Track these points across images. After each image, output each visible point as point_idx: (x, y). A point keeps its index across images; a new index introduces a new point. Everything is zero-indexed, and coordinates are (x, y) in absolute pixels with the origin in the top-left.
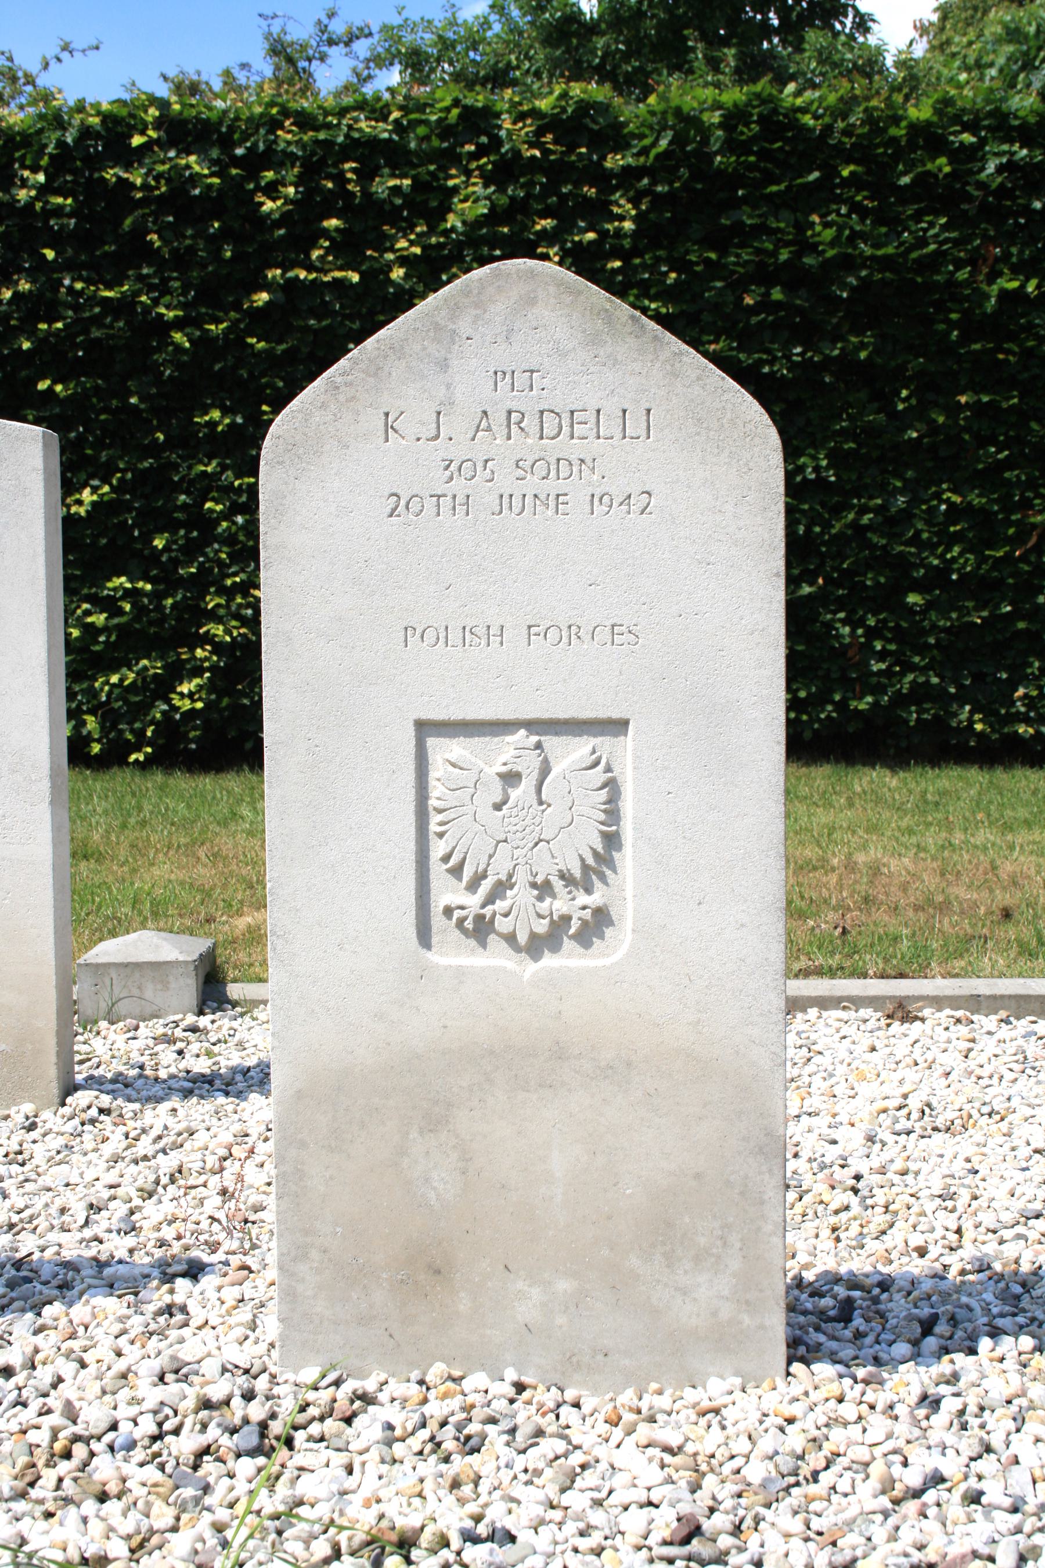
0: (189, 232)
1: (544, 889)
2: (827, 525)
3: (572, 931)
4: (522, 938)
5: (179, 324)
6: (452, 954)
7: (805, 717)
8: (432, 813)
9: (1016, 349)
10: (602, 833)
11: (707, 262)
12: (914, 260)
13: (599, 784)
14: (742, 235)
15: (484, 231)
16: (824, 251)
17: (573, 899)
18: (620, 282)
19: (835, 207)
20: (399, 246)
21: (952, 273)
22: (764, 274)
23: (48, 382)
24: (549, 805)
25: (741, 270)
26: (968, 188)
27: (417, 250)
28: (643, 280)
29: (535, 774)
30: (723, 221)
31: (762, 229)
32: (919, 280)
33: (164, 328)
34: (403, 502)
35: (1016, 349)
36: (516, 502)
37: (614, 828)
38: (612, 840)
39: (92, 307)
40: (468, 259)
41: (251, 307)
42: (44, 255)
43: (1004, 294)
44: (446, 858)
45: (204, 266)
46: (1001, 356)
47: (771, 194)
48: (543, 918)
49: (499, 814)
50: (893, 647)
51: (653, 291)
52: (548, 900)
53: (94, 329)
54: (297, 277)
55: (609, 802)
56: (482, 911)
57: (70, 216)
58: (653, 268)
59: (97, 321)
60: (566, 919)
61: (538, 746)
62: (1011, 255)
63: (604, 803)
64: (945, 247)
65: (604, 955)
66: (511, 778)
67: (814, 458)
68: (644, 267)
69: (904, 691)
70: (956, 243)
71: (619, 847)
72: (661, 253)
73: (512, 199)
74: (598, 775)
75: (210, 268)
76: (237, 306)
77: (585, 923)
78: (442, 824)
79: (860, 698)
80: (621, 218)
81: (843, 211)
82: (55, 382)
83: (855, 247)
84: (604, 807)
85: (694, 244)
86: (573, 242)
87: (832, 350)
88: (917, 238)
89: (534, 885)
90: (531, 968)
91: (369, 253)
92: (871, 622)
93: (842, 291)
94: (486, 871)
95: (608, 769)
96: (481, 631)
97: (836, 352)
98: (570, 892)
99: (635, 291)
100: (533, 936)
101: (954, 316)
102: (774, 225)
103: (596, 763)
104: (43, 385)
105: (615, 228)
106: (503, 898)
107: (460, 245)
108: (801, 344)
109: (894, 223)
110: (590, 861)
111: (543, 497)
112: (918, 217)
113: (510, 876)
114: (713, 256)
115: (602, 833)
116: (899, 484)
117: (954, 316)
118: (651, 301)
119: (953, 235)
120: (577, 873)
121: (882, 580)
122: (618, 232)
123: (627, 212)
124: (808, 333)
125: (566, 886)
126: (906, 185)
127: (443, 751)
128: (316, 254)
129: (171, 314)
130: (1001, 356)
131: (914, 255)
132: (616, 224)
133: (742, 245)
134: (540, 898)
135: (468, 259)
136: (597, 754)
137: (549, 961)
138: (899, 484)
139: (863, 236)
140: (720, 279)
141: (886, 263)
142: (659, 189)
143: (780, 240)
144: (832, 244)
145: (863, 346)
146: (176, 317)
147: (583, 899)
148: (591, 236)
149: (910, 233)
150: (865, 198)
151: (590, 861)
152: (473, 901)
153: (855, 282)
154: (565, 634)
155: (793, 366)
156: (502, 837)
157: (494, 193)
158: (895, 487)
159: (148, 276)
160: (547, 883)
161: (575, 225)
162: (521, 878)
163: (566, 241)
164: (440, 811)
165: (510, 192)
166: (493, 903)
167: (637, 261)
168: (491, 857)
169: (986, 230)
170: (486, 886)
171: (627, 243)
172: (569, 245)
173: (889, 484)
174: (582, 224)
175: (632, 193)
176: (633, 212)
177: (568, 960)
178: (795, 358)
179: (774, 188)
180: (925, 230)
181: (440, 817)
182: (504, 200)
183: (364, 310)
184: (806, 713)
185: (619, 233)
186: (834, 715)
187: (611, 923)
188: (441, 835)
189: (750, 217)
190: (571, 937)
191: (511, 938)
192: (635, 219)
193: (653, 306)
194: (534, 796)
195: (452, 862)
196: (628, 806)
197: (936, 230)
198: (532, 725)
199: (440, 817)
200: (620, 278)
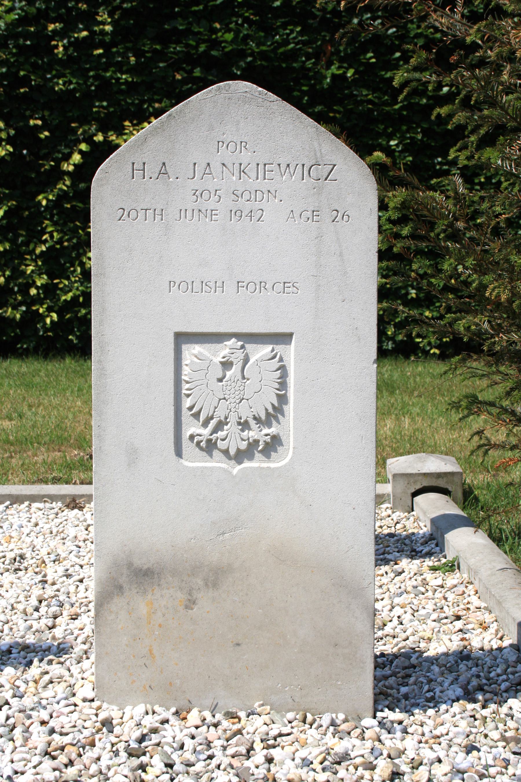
3: (260, 448)
4: (232, 452)
6: (194, 461)
9: (342, 109)
10: (277, 395)
11: (155, 51)
12: (282, 53)
13: (275, 369)
14: (178, 36)
15: (20, 29)
16: (225, 47)
17: (261, 431)
21: (304, 62)
24: (248, 379)
25: (176, 57)
26: (313, 10)
28: (118, 62)
29: (240, 364)
31: (188, 32)
32: (284, 65)
34: (126, 213)
35: (342, 109)
36: (189, 213)
37: (283, 392)
38: (283, 399)
43: (334, 76)
44: (191, 408)
46: (331, 115)
47: (195, 11)
48: (245, 440)
51: (124, 68)
52: (246, 432)
56: (211, 437)
60: (257, 442)
61: (243, 347)
62: (340, 51)
63: (278, 379)
64: (298, 47)
66: (227, 365)
70: (304, 43)
72: (129, 45)
73: (39, 10)
74: (275, 364)
77: (266, 443)
80: (104, 23)
81: (240, 22)
83: (248, 44)
84: (279, 380)
86: (74, 37)
88: (283, 40)
89: (239, 424)
94: (213, 415)
96: (212, 284)
98: (259, 427)
99: (113, 69)
100: (239, 451)
101: (305, 88)
102: (196, 30)
105: (100, 30)
106: (222, 430)
109: (270, 31)
110: (271, 410)
111: (203, 211)
112: (284, 26)
113: (226, 418)
114: (158, 47)
115: (277, 395)
117: (305, 88)
119: (305, 38)
120: (263, 417)
123: (105, 19)
125: (257, 424)
126: (278, 7)
127: (191, 352)
130: (331, 115)
131: (281, 50)
132: (101, 27)
134: (243, 430)
136: (275, 352)
137: (247, 464)
141: (263, 55)
142: (125, 5)
143: (200, 39)
144: (233, 41)
147: (266, 431)
148: (85, 33)
149: (280, 36)
151: (271, 410)
152: (206, 432)
153: (244, 65)
154: (258, 287)
156: (222, 397)
157: (25, 5)
160: (246, 422)
161: (77, 27)
162: (233, 419)
164: (187, 382)
165: (37, 5)
167: (114, 50)
168: (216, 408)
169: (325, 36)
171: (107, 39)
172: (73, 39)
175: (110, 8)
176: (109, 20)
177: (257, 463)
179: (196, 8)
180: (288, 35)
181: (187, 386)
182: (33, 10)
185: (103, 33)
188: (188, 396)
189: (181, 25)
190: (261, 452)
191: (226, 452)
194: (240, 373)
195: (194, 410)
196: (291, 380)
197: (294, 35)
198: (238, 336)
199: (187, 386)
200: (104, 60)
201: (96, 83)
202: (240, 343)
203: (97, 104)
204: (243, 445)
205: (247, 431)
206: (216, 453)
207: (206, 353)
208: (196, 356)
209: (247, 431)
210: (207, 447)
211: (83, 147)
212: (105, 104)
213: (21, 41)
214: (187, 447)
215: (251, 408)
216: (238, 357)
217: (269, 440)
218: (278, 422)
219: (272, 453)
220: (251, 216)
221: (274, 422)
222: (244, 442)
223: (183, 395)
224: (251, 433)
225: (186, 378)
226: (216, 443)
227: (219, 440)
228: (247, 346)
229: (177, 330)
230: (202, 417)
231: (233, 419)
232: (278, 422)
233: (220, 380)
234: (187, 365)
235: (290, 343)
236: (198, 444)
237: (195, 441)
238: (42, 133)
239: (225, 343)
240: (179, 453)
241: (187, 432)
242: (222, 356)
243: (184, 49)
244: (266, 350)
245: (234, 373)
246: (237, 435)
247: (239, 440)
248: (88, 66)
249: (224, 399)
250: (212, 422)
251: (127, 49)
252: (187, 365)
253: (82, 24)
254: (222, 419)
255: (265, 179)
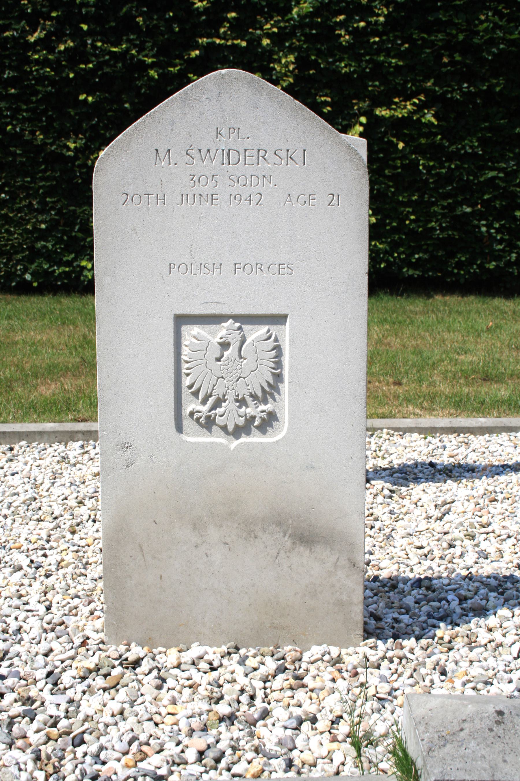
0: (155, 17)
1: (242, 402)
2: (476, 177)
3: (256, 423)
4: (230, 428)
5: (152, 66)
6: (195, 437)
7: (462, 272)
8: (183, 363)
11: (423, 39)
13: (270, 349)
14: (439, 26)
17: (257, 407)
18: (376, 49)
19: (485, 12)
20: (265, 27)
22: (450, 46)
23: (85, 96)
24: (245, 359)
27: (275, 30)
29: (238, 344)
30: (429, 18)
31: (450, 23)
33: (144, 67)
37: (279, 370)
38: (278, 377)
39: (104, 56)
40: (298, 34)
41: (189, 58)
42: (82, 28)
44: (190, 387)
45: (163, 36)
47: (457, 5)
48: (242, 417)
49: (219, 363)
50: (507, 237)
53: (105, 68)
54: (215, 42)
55: (275, 357)
57: (93, 6)
58: (393, 42)
59: (106, 63)
60: (253, 418)
61: (240, 328)
65: (271, 436)
66: (225, 345)
67: (471, 141)
68: (388, 40)
69: (512, 260)
71: (282, 382)
75: (166, 37)
76: (181, 57)
77: (263, 420)
78: (188, 369)
79: (489, 263)
80: (378, 15)
82: (88, 95)
85: (415, 30)
86: (353, 27)
87: (483, 86)
89: (237, 401)
90: (235, 443)
91: (250, 30)
92: (497, 226)
93: (489, 56)
94: (211, 393)
95: (276, 340)
96: (211, 267)
97: (485, 88)
100: (237, 427)
102: (457, 21)
103: (269, 338)
104: (82, 97)
106: (221, 407)
107: (294, 27)
108: (467, 83)
111: (204, 195)
114: (425, 36)
116: (511, 155)
118: (393, 58)
120: (260, 394)
121: (504, 203)
122: (376, 22)
124: (471, 77)
127: (191, 333)
128: (222, 30)
129: (150, 60)
133: (439, 31)
134: (240, 407)
135: (298, 34)
137: (244, 439)
138: (511, 155)
139: (500, 28)
140: (428, 48)
145: (498, 84)
146: (153, 62)
147: (262, 407)
148: (362, 24)
150: (503, 8)
152: (205, 409)
155: (463, 94)
158: (509, 156)
159: (133, 40)
161: (353, 18)
162: (230, 396)
163: (349, 26)
164: (187, 362)
166: (216, 409)
168: (214, 386)
170: (211, 401)
172: (351, 29)
173: (506, 155)
174: (357, 18)
177: (256, 438)
178: (464, 90)
181: (187, 365)
183: (245, 61)
184: (463, 270)
186: (477, 270)
187: (277, 420)
190: (258, 427)
191: (224, 428)
192: (385, 16)
193: (393, 61)
194: (237, 353)
196: (286, 360)
198: (236, 318)
199: (187, 365)
201: (370, 66)
202: (237, 325)
203: (370, 83)
204: (241, 421)
205: (244, 407)
206: (215, 428)
207: (204, 334)
208: (195, 337)
209: (244, 407)
210: (206, 423)
211: (363, 120)
212: (377, 83)
213: (307, 30)
214: (187, 422)
215: (248, 386)
216: (235, 338)
217: (265, 416)
218: (275, 400)
219: (268, 428)
220: (250, 200)
221: (270, 400)
222: (241, 418)
223: (183, 373)
224: (248, 410)
225: (186, 358)
226: (215, 418)
227: (217, 416)
228: (243, 326)
229: (178, 312)
230: (201, 395)
231: (230, 396)
232: (275, 400)
233: (218, 360)
234: (186, 346)
235: (284, 323)
236: (198, 420)
237: (195, 417)
238: (324, 108)
239: (223, 324)
240: (179, 429)
241: (187, 409)
242: (219, 336)
243: (445, 37)
244: (262, 330)
245: (230, 354)
246: (235, 412)
247: (236, 416)
248: (362, 51)
249: (222, 377)
250: (210, 399)
251: (396, 37)
252: (186, 346)
253: (357, 16)
254: (221, 396)
255: (245, 164)
